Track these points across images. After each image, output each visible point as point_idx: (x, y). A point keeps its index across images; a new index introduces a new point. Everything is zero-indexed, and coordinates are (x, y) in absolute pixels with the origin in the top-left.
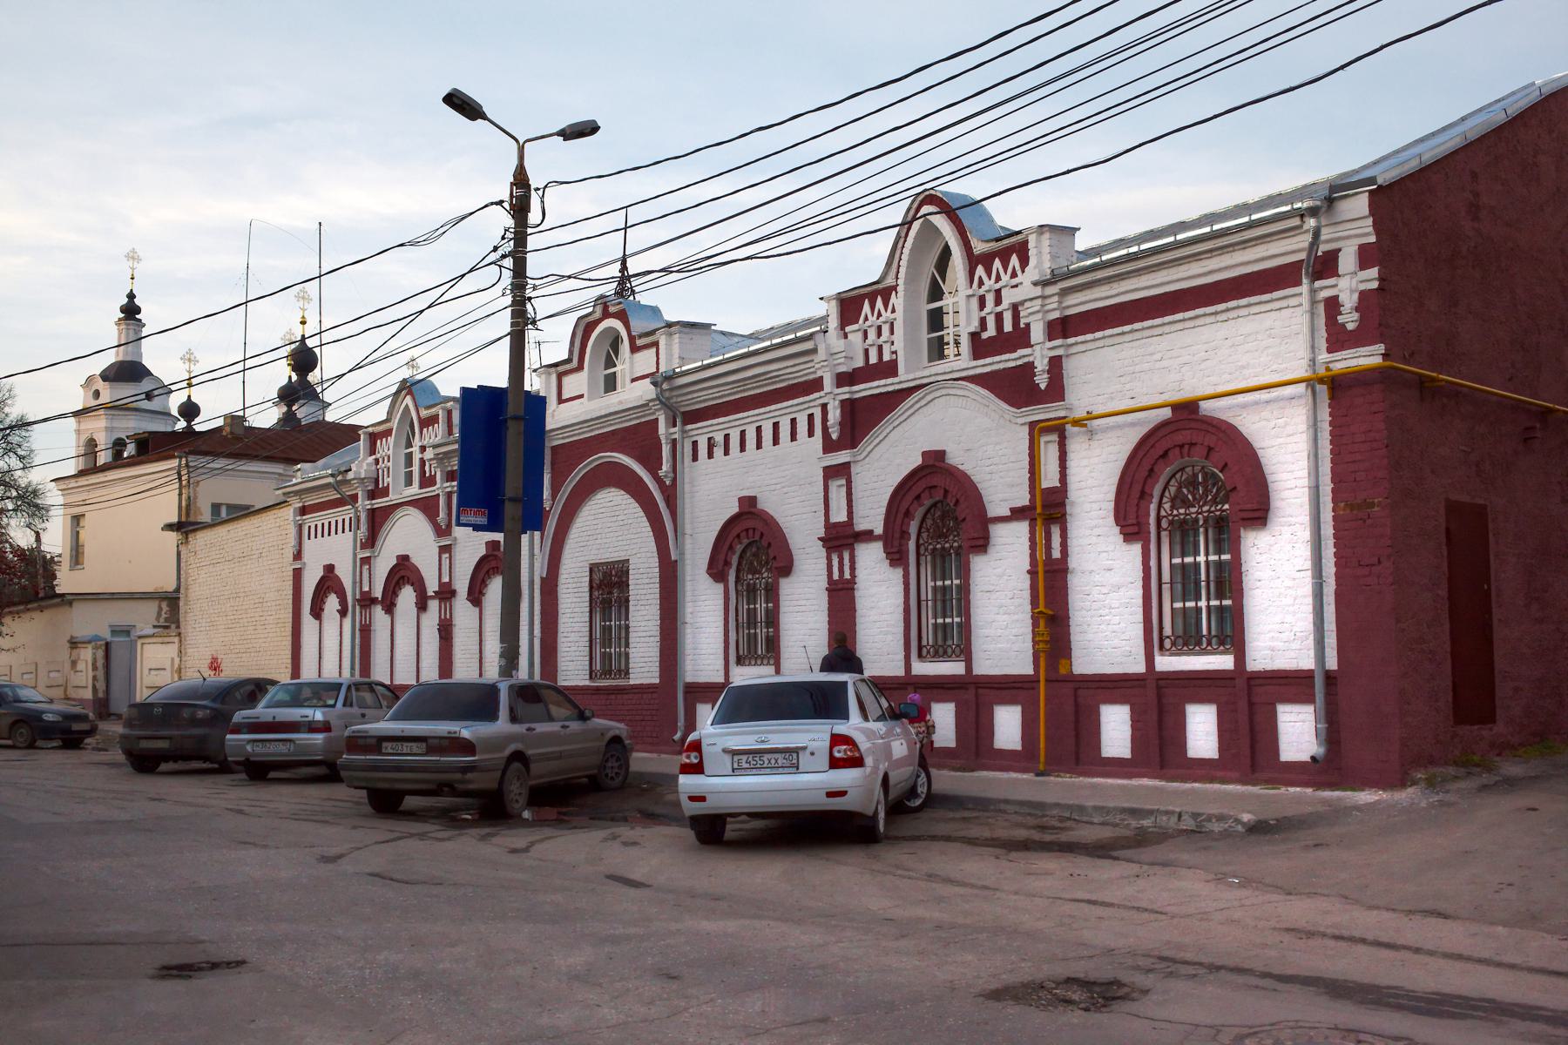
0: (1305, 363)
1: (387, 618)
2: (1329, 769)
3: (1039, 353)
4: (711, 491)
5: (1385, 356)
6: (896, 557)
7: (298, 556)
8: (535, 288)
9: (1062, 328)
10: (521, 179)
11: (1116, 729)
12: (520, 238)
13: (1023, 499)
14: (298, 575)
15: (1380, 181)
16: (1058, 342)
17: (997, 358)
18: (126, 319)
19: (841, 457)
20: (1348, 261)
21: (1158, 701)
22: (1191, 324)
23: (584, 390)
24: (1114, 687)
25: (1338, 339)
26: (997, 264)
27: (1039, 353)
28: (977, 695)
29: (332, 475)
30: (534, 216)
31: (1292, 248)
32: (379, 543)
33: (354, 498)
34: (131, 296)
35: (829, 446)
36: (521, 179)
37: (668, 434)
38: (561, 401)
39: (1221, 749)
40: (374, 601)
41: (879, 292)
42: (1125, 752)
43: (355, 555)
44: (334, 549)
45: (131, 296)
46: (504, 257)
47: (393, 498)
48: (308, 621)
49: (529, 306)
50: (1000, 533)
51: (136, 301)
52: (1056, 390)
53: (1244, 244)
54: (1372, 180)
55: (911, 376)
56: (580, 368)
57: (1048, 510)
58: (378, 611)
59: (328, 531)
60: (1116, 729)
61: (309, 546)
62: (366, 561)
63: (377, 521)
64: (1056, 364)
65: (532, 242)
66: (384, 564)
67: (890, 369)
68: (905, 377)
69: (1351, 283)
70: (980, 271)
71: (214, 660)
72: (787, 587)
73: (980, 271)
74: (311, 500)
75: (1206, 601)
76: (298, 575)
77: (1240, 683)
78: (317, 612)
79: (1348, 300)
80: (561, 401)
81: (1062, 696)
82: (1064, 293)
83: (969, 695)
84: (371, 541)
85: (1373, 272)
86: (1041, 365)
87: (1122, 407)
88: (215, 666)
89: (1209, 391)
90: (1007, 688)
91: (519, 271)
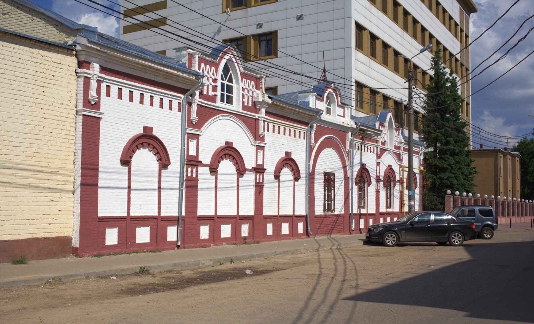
2: (307, 233)
39: (273, 233)
80: (344, 117)
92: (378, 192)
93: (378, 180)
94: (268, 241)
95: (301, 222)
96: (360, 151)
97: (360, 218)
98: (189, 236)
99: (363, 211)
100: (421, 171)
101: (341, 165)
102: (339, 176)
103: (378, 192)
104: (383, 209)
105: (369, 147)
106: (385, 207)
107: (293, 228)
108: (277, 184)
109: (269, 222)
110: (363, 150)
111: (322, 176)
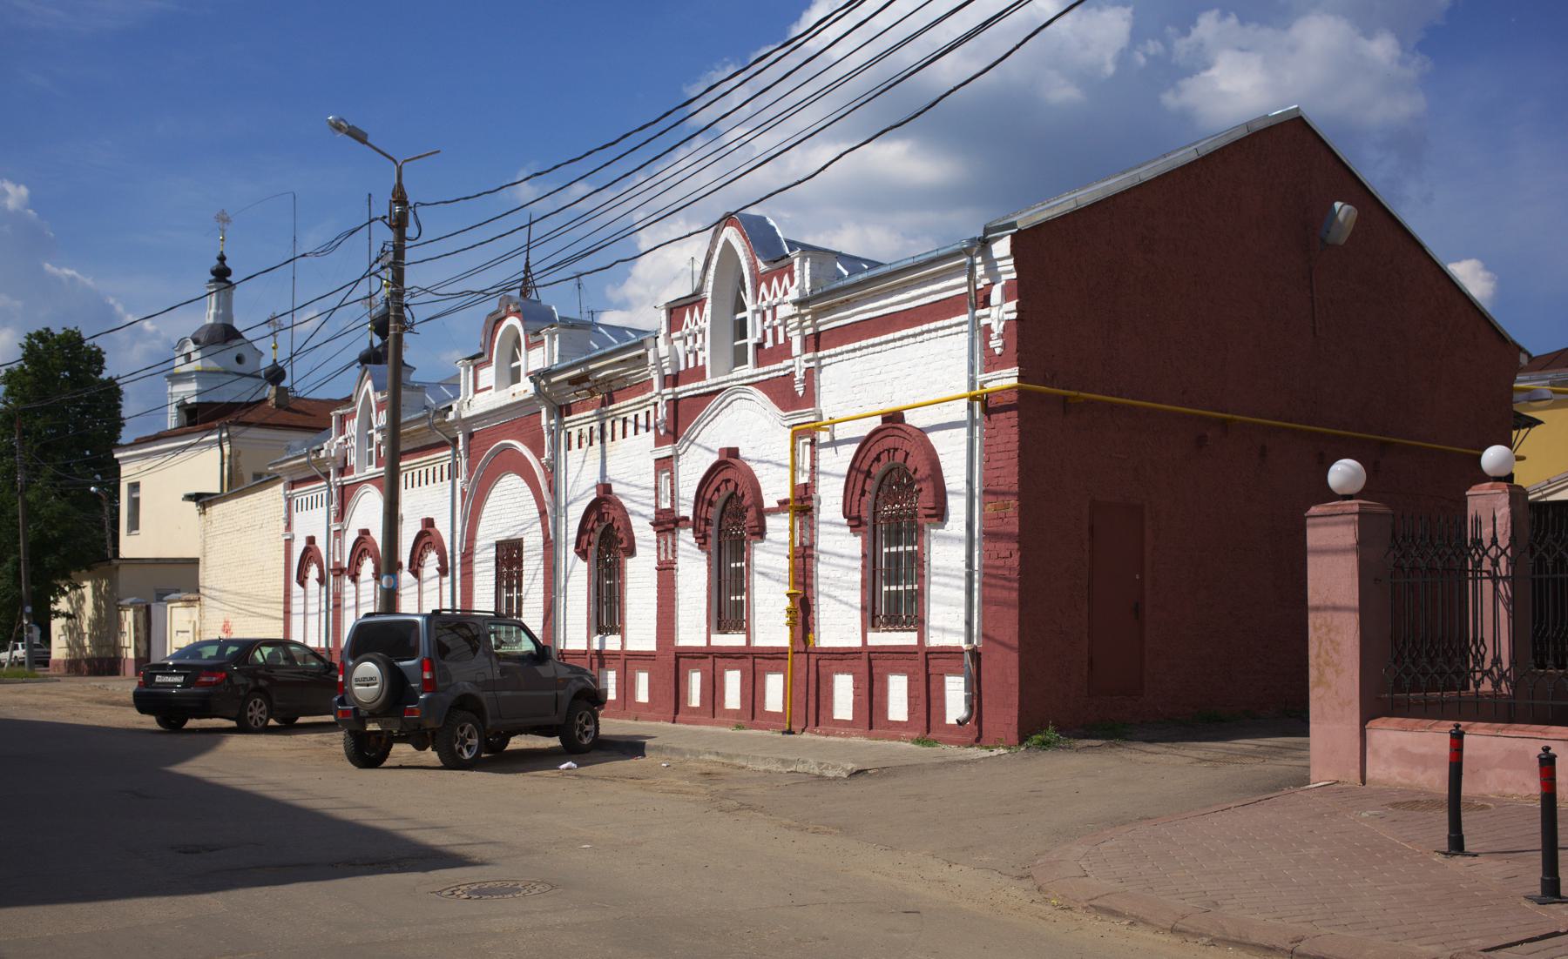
0: (965, 382)
1: (353, 587)
2: (976, 727)
3: (798, 363)
4: (580, 476)
5: (1020, 378)
6: (702, 540)
7: (289, 527)
8: (412, 295)
9: (816, 342)
10: (400, 197)
11: (844, 691)
12: (399, 252)
13: (786, 494)
14: (288, 544)
15: (1019, 226)
16: (810, 355)
17: (772, 367)
18: (217, 281)
19: (667, 451)
20: (996, 294)
21: (870, 667)
22: (899, 343)
23: (493, 383)
24: (841, 656)
25: (992, 362)
26: (775, 282)
27: (798, 363)
28: (755, 662)
29: (306, 455)
30: (411, 231)
31: (956, 285)
32: (347, 518)
33: (327, 475)
34: (222, 259)
35: (659, 442)
36: (400, 197)
37: (549, 426)
38: (476, 391)
39: (910, 714)
40: (342, 571)
41: (694, 301)
42: (849, 716)
43: (328, 529)
44: (313, 521)
45: (222, 259)
46: (383, 268)
47: (357, 475)
48: (296, 587)
49: (406, 312)
50: (770, 521)
51: (227, 263)
52: (810, 398)
53: (935, 278)
54: (1013, 225)
55: (715, 381)
56: (489, 362)
57: (802, 505)
58: (347, 581)
59: (311, 505)
60: (844, 691)
61: (297, 517)
62: (337, 533)
63: (345, 497)
64: (809, 373)
65: (410, 255)
66: (351, 537)
67: (699, 373)
68: (710, 382)
69: (1001, 312)
70: (763, 287)
71: (227, 623)
72: (631, 565)
73: (763, 287)
74: (297, 477)
75: (893, 592)
76: (288, 544)
77: (921, 656)
78: (302, 581)
79: (997, 328)
80: (476, 391)
81: (810, 664)
82: (816, 314)
83: (748, 663)
84: (341, 515)
85: (1012, 305)
86: (799, 375)
87: (854, 414)
88: (226, 629)
89: (910, 403)
90: (774, 656)
91: (398, 278)
92: (666, 571)
93: (666, 523)
94: (688, 723)
95: (642, 670)
96: (597, 443)
97: (602, 665)
98: (811, 704)
99: (613, 643)
100: (987, 405)
101: (535, 513)
102: (533, 542)
103: (666, 571)
104: (692, 630)
105: (631, 417)
106: (856, 618)
107: (927, 700)
108: (416, 588)
109: (695, 668)
110: (608, 438)
111: (492, 553)
